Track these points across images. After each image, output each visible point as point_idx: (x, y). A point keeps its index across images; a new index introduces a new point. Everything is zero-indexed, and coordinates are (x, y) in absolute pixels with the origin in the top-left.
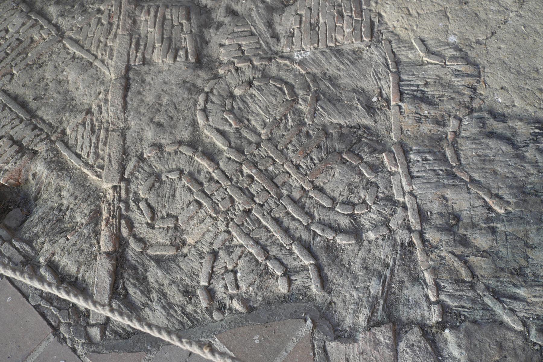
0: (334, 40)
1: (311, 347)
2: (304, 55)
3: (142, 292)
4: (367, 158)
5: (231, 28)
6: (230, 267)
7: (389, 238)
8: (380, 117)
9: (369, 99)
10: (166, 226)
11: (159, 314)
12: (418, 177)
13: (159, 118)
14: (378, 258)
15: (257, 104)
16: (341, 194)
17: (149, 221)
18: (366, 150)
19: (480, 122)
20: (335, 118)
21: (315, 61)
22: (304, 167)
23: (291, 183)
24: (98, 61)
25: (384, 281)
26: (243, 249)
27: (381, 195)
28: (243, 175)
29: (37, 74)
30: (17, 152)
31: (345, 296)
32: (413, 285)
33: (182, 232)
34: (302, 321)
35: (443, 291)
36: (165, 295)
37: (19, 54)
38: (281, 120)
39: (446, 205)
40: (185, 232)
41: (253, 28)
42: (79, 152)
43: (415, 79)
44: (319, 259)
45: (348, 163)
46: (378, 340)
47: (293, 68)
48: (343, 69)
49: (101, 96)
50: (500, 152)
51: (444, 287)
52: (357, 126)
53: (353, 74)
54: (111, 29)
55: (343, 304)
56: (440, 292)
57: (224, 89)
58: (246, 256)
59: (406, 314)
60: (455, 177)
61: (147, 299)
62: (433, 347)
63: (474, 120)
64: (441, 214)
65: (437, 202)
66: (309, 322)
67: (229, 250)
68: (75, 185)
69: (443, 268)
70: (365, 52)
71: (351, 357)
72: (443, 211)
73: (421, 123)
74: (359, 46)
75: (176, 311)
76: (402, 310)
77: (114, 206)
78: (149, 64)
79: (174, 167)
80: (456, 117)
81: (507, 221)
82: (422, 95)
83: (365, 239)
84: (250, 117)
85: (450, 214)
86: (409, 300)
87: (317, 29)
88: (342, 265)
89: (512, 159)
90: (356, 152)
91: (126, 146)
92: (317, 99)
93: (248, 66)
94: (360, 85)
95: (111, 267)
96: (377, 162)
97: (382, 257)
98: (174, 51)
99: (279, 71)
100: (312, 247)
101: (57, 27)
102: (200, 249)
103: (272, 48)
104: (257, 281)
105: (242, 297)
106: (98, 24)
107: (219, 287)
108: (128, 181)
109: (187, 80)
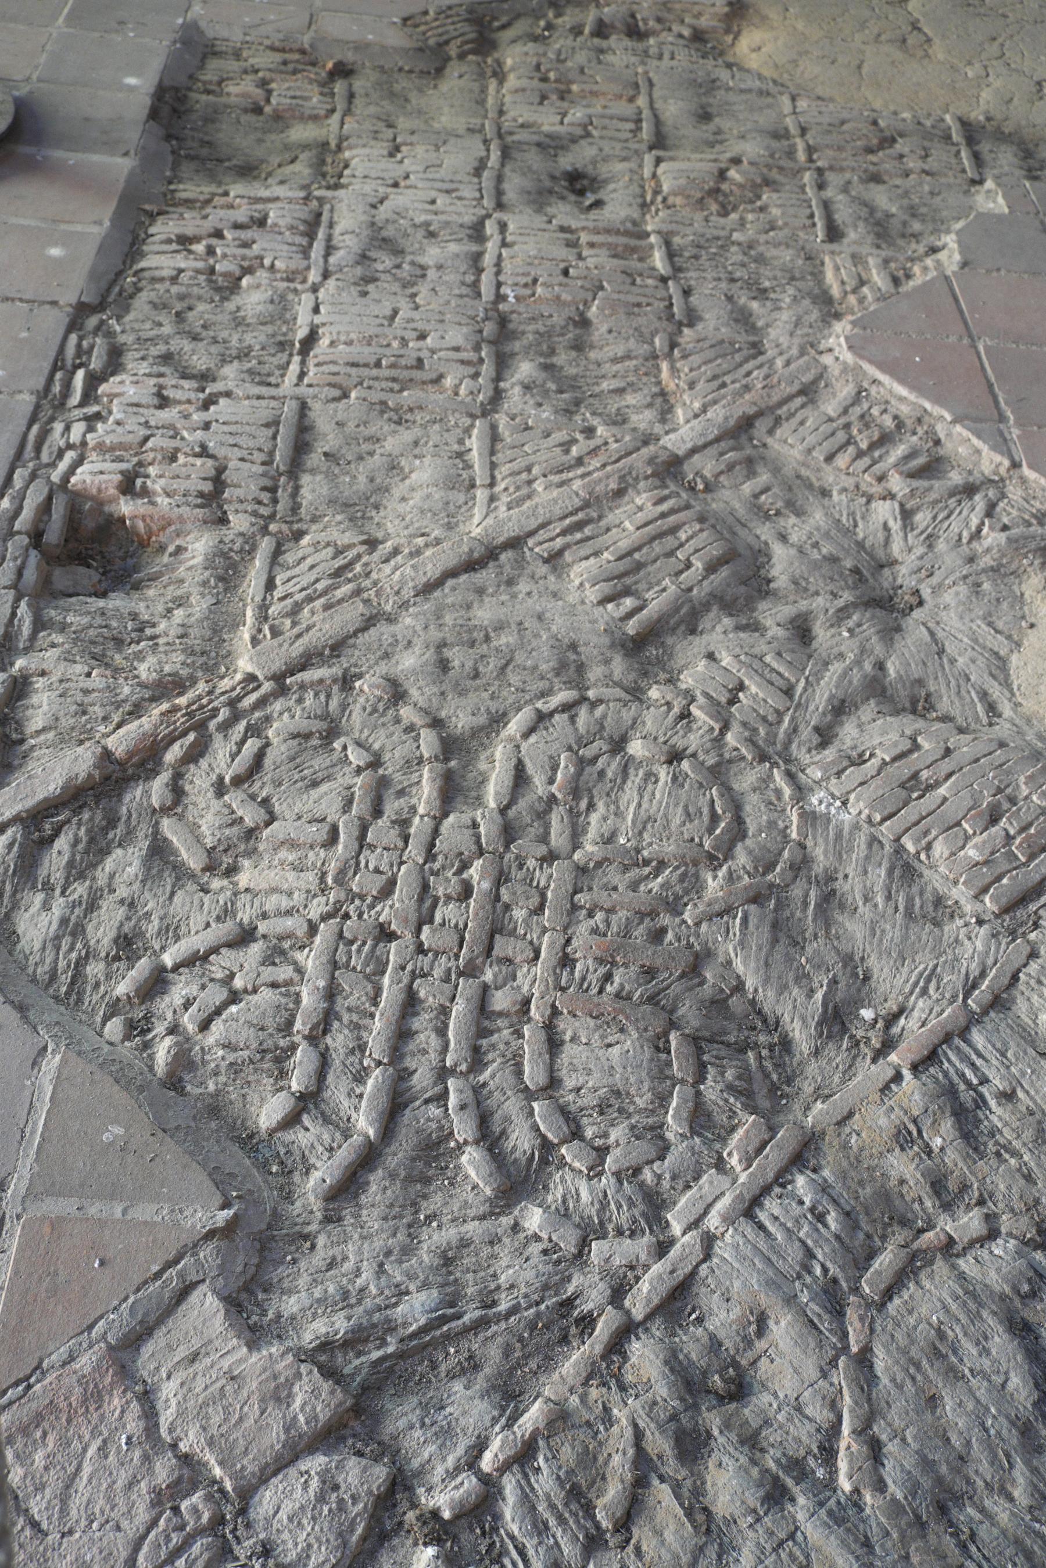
0: (924, 842)
1: (171, 1257)
2: (833, 811)
3: (71, 864)
4: (711, 1090)
5: (764, 648)
6: (238, 983)
7: (558, 1262)
8: (838, 1055)
9: (859, 1003)
10: (240, 813)
11: (46, 923)
12: (761, 1227)
13: (456, 656)
14: (491, 1271)
15: (641, 797)
16: (579, 1089)
17: (227, 780)
18: (730, 1075)
19: (1029, 1281)
20: (745, 962)
21: (840, 843)
22: (577, 975)
23: (519, 974)
24: (312, 297)
25: (444, 1320)
26: (296, 977)
27: (647, 1175)
28: (460, 872)
29: (379, 426)
30: (201, 494)
31: (345, 1258)
32: (485, 1394)
33: (250, 853)
34: (218, 1200)
35: (526, 1476)
36: (92, 906)
37: (394, 380)
38: (646, 862)
39: (749, 1343)
40: (255, 857)
41: (802, 683)
42: (278, 582)
43: (994, 1062)
44: (389, 1145)
45: (664, 1056)
46: (290, 1395)
47: (784, 810)
48: (876, 906)
49: (420, 541)
50: (998, 1380)
51: (538, 1469)
52: (771, 1021)
53: (883, 931)
54: (570, 468)
55: (323, 1265)
56: (516, 1468)
57: (619, 721)
58: (287, 995)
59: (402, 1423)
60: (838, 1312)
61: (62, 881)
62: (368, 1545)
63: (1021, 1263)
64: (715, 1344)
65: (736, 1312)
66: (224, 1216)
67: (275, 955)
68: (207, 618)
69: (582, 1434)
70: (959, 922)
71: (208, 1361)
72: (728, 1344)
73: (903, 1149)
74: (963, 901)
75: (71, 949)
76: (406, 1408)
77: (211, 702)
78: (554, 569)
79: (376, 746)
80: (989, 1218)
81: (830, 1513)
82: (970, 1104)
83: (516, 1212)
84: (601, 806)
85: (735, 1364)
86: (442, 1408)
87: (915, 795)
88: (414, 1204)
89: (1002, 1420)
90: (706, 1058)
91: (351, 641)
92: (756, 899)
93: (712, 729)
94: (872, 962)
95: (83, 775)
96: (721, 1118)
97: (503, 1279)
98: (619, 587)
99: (754, 790)
100: (407, 1112)
101: (498, 396)
102: (239, 904)
103: (794, 746)
104: (245, 1054)
105: (190, 1050)
106: (561, 445)
107: (179, 990)
108: (282, 690)
109: (581, 649)
